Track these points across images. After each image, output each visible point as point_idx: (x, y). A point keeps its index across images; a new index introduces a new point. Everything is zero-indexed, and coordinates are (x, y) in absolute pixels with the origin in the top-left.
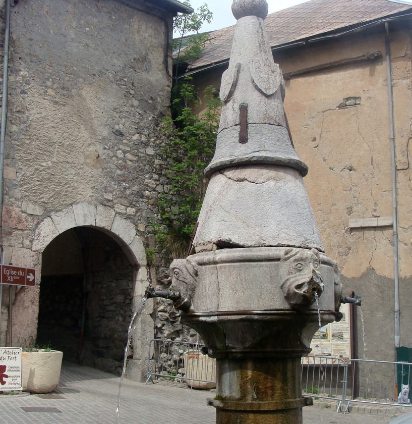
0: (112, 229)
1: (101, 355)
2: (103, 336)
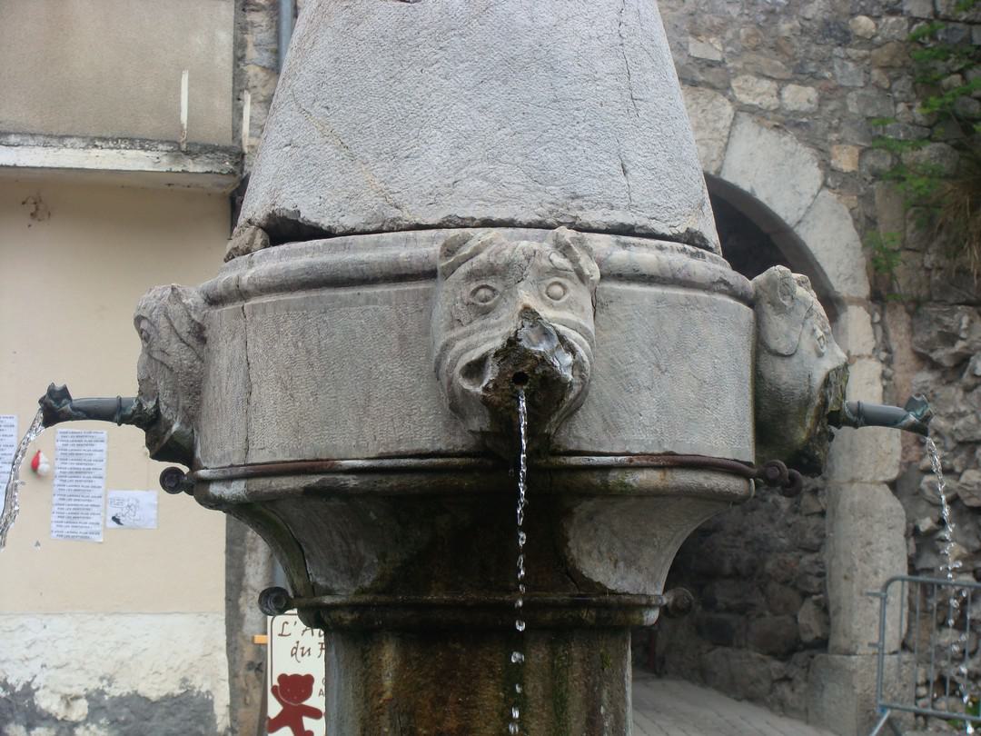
0: (726, 167)
1: (722, 636)
2: (727, 568)
